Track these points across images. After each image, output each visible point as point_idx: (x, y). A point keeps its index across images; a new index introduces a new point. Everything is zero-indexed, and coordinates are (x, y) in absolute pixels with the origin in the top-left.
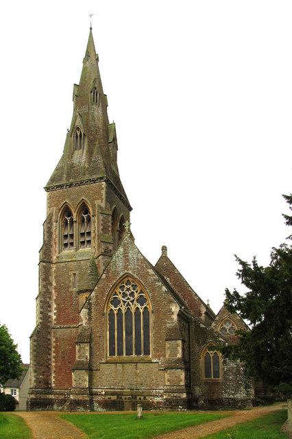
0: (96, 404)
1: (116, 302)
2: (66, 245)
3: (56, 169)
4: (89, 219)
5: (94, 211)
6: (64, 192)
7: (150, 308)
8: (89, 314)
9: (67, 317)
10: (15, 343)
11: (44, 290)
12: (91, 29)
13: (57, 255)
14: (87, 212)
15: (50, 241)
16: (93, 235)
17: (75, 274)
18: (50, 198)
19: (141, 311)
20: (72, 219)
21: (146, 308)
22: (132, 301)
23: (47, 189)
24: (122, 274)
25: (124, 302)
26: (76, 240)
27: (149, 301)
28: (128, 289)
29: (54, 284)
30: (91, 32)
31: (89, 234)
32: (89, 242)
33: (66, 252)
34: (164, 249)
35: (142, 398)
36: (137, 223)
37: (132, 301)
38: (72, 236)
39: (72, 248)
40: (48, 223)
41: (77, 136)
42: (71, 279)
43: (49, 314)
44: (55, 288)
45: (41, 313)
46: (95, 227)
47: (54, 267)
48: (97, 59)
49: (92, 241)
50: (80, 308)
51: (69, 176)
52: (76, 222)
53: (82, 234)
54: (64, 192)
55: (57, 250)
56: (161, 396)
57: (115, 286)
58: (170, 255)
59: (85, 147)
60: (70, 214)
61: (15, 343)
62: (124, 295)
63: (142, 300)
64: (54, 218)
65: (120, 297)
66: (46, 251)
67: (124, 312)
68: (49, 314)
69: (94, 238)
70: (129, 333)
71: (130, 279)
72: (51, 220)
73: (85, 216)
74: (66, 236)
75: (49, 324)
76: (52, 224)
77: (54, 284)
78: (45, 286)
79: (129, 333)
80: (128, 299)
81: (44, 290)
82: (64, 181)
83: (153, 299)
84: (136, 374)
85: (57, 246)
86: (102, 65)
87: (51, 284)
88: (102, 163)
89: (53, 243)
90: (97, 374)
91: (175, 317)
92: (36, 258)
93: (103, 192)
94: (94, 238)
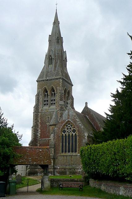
0: (56, 173)
1: (64, 132)
2: (45, 104)
3: (41, 73)
4: (55, 94)
5: (57, 91)
6: (44, 83)
7: (77, 134)
8: (54, 136)
9: (45, 134)
10: (9, 126)
11: (36, 124)
12: (56, 10)
13: (41, 109)
14: (54, 91)
15: (38, 103)
16: (56, 101)
17: (48, 117)
18: (38, 85)
19: (74, 135)
20: (47, 94)
21: (75, 134)
22: (71, 131)
23: (37, 81)
24: (67, 121)
25: (68, 131)
26: (49, 102)
27: (77, 131)
28: (69, 127)
29: (40, 121)
30: (56, 11)
31: (55, 100)
32: (54, 103)
33: (46, 107)
34: (86, 103)
35: (73, 170)
36: (76, 91)
37: (71, 131)
38: (47, 101)
39: (47, 106)
40: (38, 96)
41: (50, 59)
42: (47, 119)
43: (37, 134)
44: (40, 123)
45: (34, 134)
46: (57, 98)
47: (40, 114)
48: (59, 23)
49: (56, 103)
50: (50, 134)
51: (47, 76)
52: (49, 95)
53: (52, 100)
54: (44, 83)
55: (41, 106)
56: (81, 169)
57: (64, 125)
58: (89, 106)
59: (53, 64)
60: (47, 92)
61: (9, 126)
62: (68, 129)
63: (74, 131)
64: (40, 93)
65: (66, 129)
66: (36, 108)
67: (67, 135)
68: (37, 134)
69: (57, 102)
70: (69, 144)
71: (70, 123)
72: (39, 94)
73: (53, 93)
74: (45, 101)
75: (37, 138)
76: (39, 96)
77: (40, 121)
78: (36, 122)
79: (69, 144)
80: (69, 130)
81: (36, 124)
82: (44, 79)
83: (78, 131)
84: (71, 160)
85: (41, 105)
86: (61, 26)
87: (38, 121)
88: (60, 71)
89: (39, 104)
90: (57, 161)
91: (86, 138)
92: (32, 110)
93: (61, 83)
94: (57, 102)
